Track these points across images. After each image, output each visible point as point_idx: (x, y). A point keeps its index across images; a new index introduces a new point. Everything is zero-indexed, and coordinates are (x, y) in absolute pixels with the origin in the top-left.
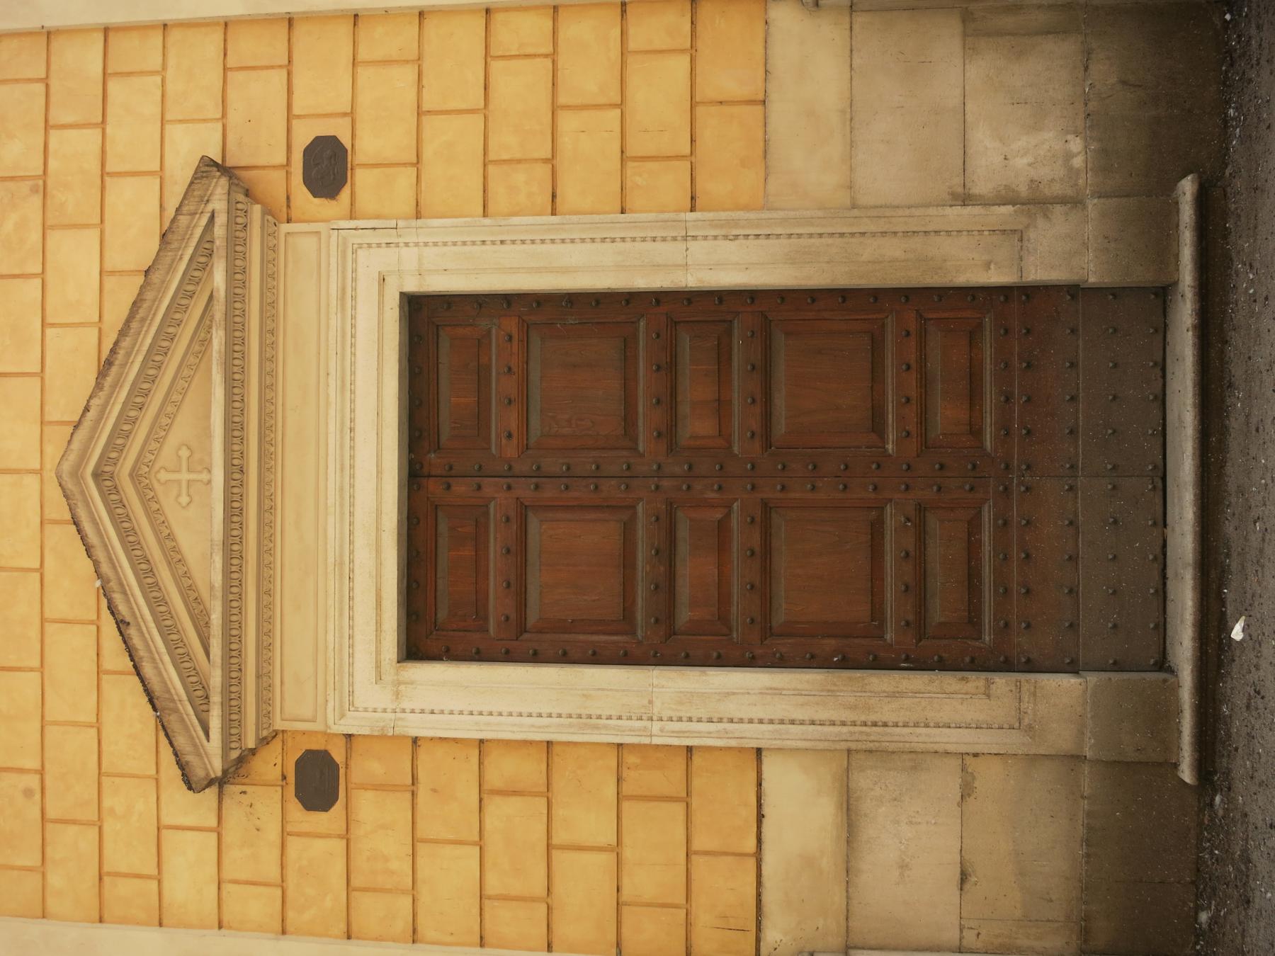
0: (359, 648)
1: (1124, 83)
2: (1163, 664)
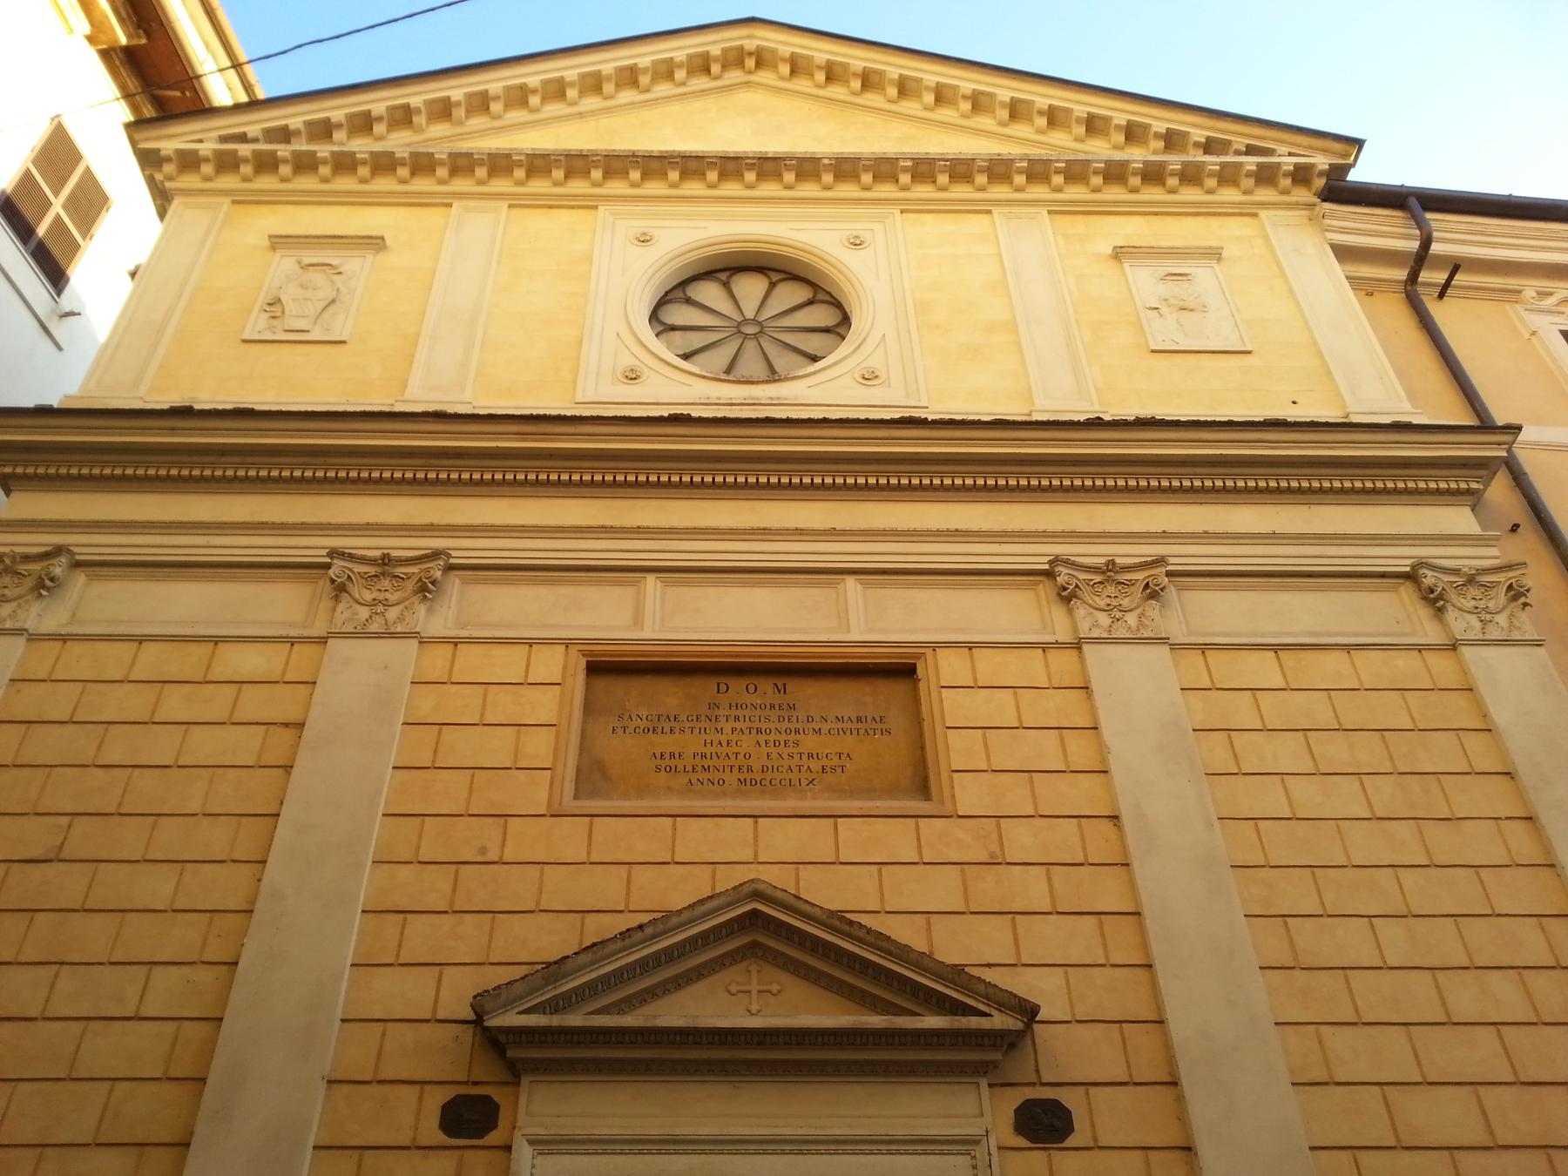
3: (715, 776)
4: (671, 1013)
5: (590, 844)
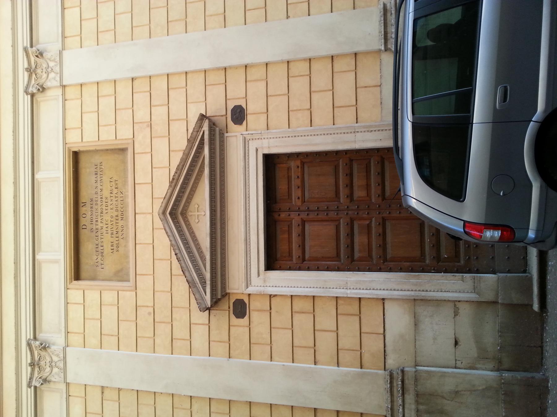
2: (525, 269)
3: (120, 229)
4: (205, 242)
5: (147, 275)
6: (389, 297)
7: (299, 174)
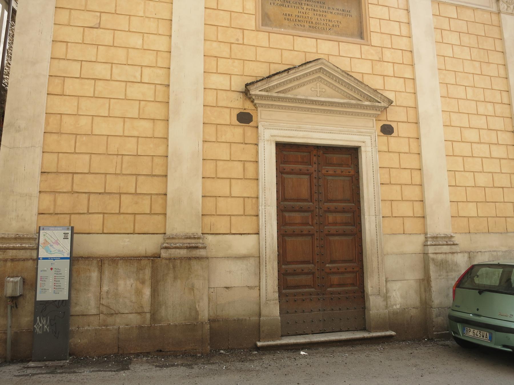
0: (279, 131)
1: (411, 317)
3: (302, 24)
5: (269, 41)
6: (261, 238)
7: (344, 173)
